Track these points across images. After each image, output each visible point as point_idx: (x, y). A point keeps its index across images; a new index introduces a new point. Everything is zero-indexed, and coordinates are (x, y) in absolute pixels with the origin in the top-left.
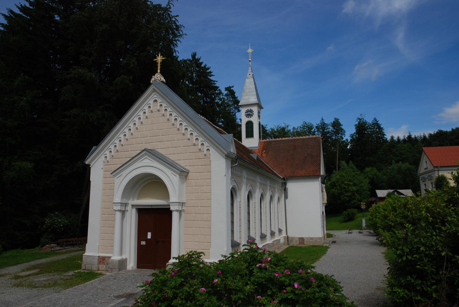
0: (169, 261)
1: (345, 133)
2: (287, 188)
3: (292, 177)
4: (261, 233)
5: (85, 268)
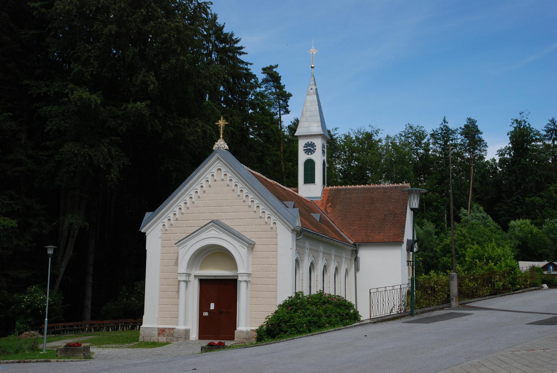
1: (487, 149)
2: (359, 257)
3: (366, 242)
5: (144, 340)
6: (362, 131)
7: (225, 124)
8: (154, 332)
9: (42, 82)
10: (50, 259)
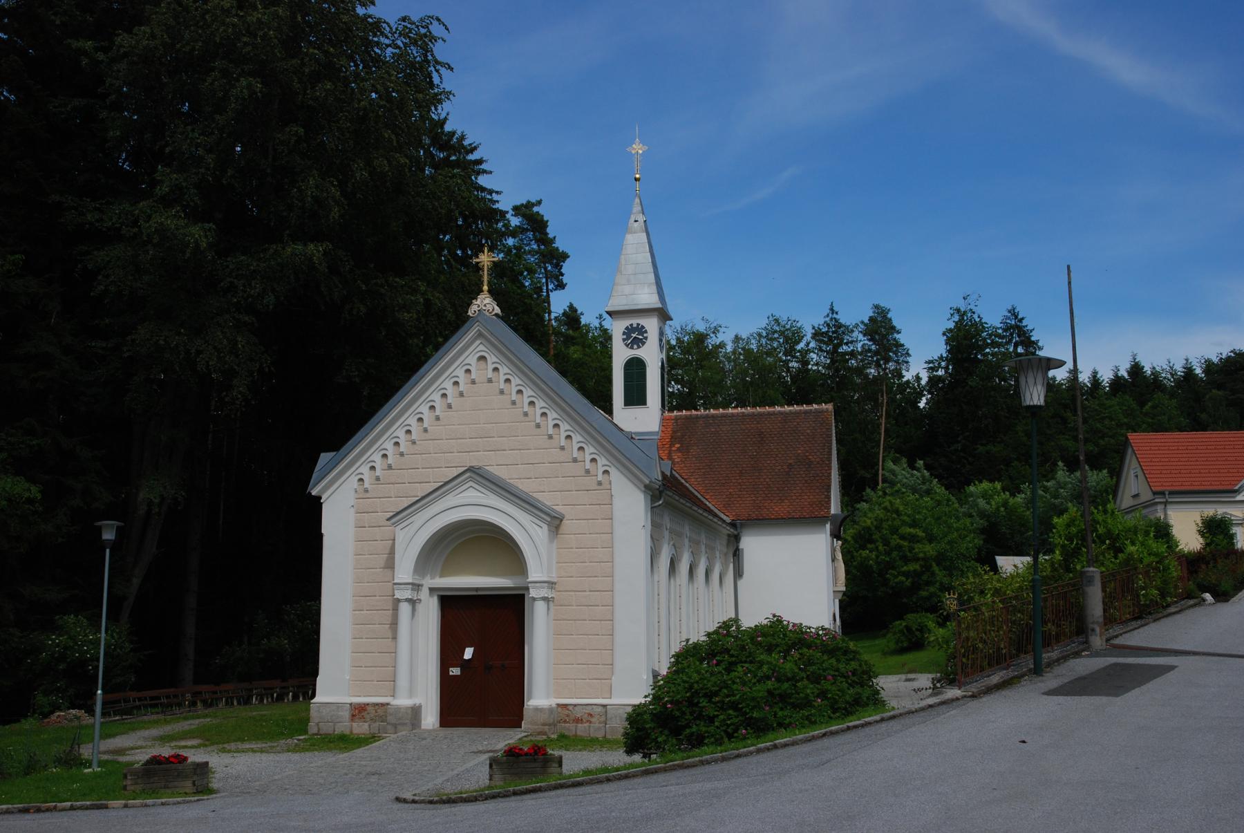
1: (909, 359)
3: (756, 519)
5: (318, 731)
6: (689, 328)
7: (491, 261)
8: (342, 713)
9: (88, 200)
10: (108, 551)
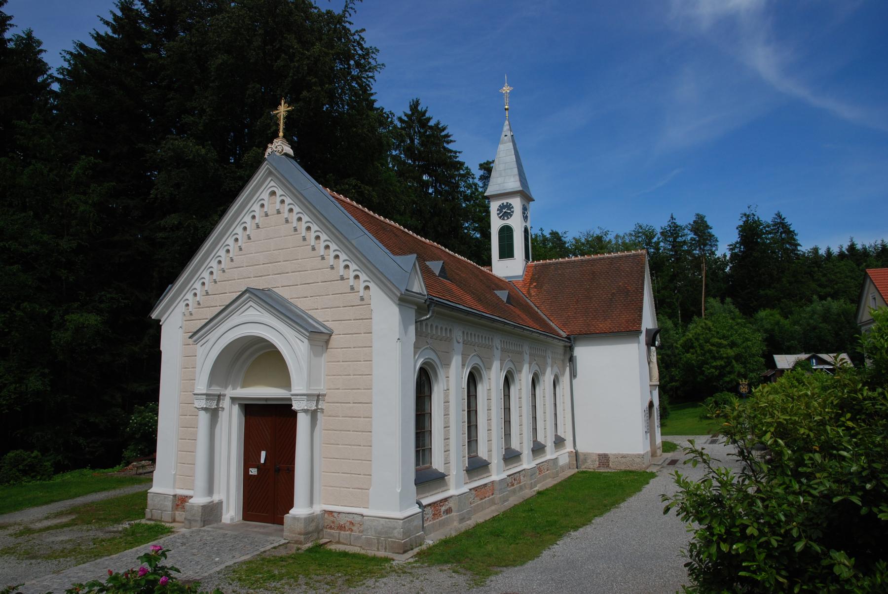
0: (290, 512)
1: (718, 243)
2: (576, 356)
3: (585, 334)
4: (555, 435)
6: (591, 233)
